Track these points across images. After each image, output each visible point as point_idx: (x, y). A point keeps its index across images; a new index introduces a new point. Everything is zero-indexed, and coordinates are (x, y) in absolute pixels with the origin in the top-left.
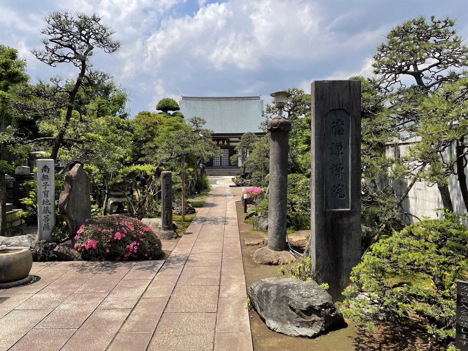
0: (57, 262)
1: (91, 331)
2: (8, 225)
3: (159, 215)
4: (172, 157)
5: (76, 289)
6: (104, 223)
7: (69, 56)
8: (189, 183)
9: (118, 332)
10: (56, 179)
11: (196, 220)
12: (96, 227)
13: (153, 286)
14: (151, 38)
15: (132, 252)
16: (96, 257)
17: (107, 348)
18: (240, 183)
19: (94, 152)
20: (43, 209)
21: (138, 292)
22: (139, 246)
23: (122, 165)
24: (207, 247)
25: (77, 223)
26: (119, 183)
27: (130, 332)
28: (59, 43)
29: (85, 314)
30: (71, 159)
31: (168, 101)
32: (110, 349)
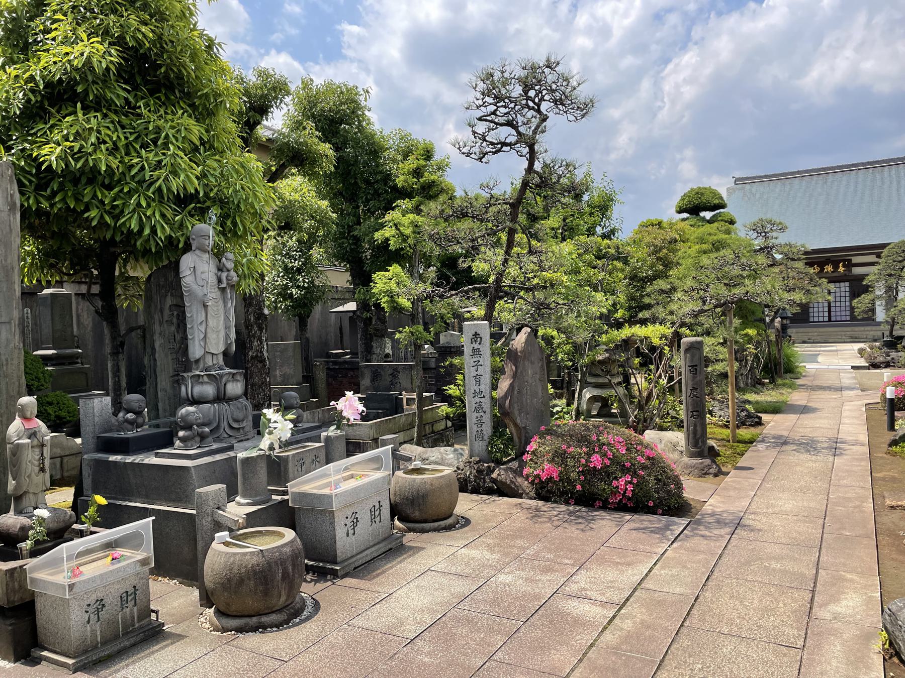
0: (497, 498)
1: (545, 630)
2: (428, 429)
3: (680, 426)
4: (706, 308)
5: (524, 549)
6: (571, 436)
7: (508, 141)
8: (747, 361)
9: (592, 645)
10: (493, 355)
11: (763, 441)
12: (558, 443)
13: (662, 568)
14: (670, 67)
15: (624, 495)
16: (560, 497)
17: (572, 670)
18: (881, 359)
19: (552, 306)
20: (474, 405)
21: (634, 575)
22: (637, 485)
23: (606, 327)
24: (787, 503)
25: (527, 433)
26: (600, 362)
27: (615, 650)
28: (492, 121)
29: (537, 597)
30: (513, 320)
31: (699, 193)
32: (577, 673)
